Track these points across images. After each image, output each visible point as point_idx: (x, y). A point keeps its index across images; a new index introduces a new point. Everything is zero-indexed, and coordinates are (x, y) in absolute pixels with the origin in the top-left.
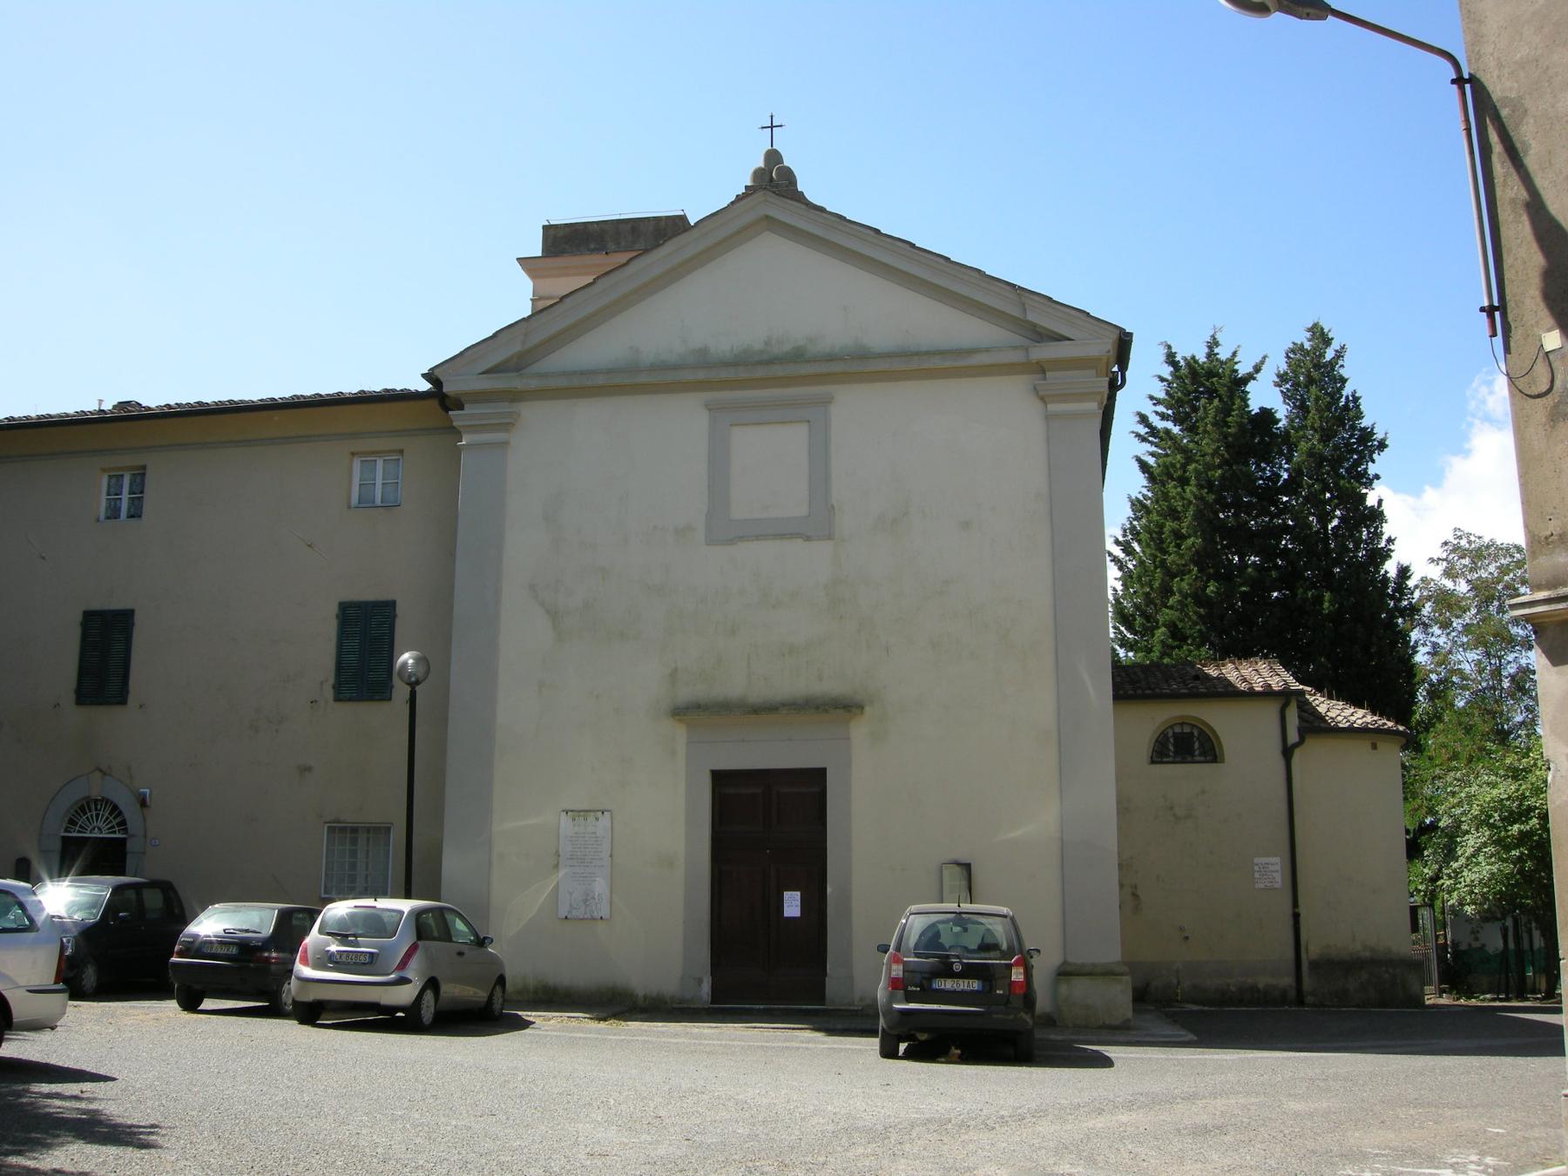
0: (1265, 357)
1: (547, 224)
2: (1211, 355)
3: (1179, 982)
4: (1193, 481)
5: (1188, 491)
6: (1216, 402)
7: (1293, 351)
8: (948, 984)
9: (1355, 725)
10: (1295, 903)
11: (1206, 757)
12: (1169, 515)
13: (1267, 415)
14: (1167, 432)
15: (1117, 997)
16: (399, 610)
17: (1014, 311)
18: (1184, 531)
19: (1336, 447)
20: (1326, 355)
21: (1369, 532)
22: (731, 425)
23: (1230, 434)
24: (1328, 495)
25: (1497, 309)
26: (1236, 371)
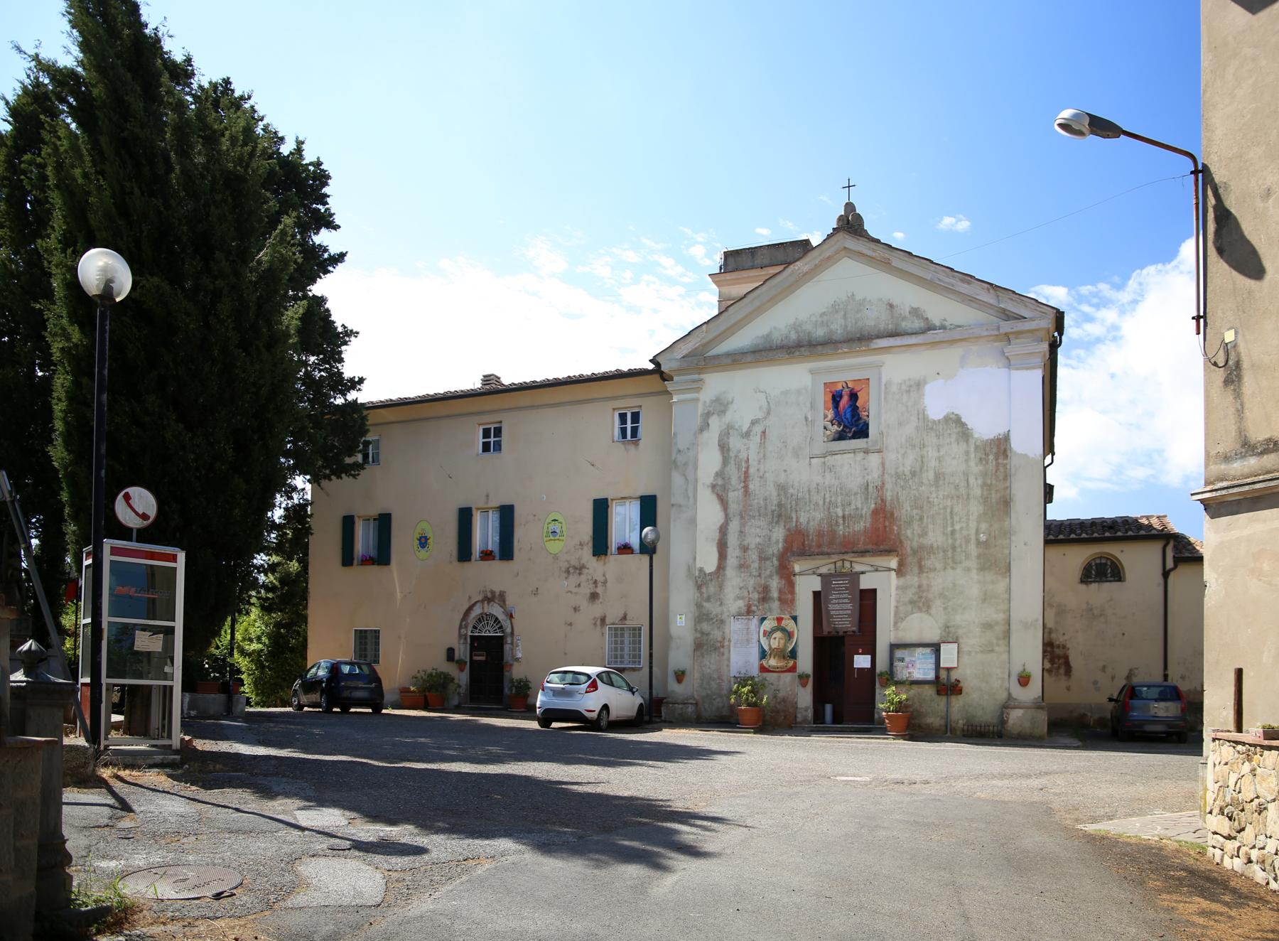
10: (1166, 667)
25: (1202, 317)
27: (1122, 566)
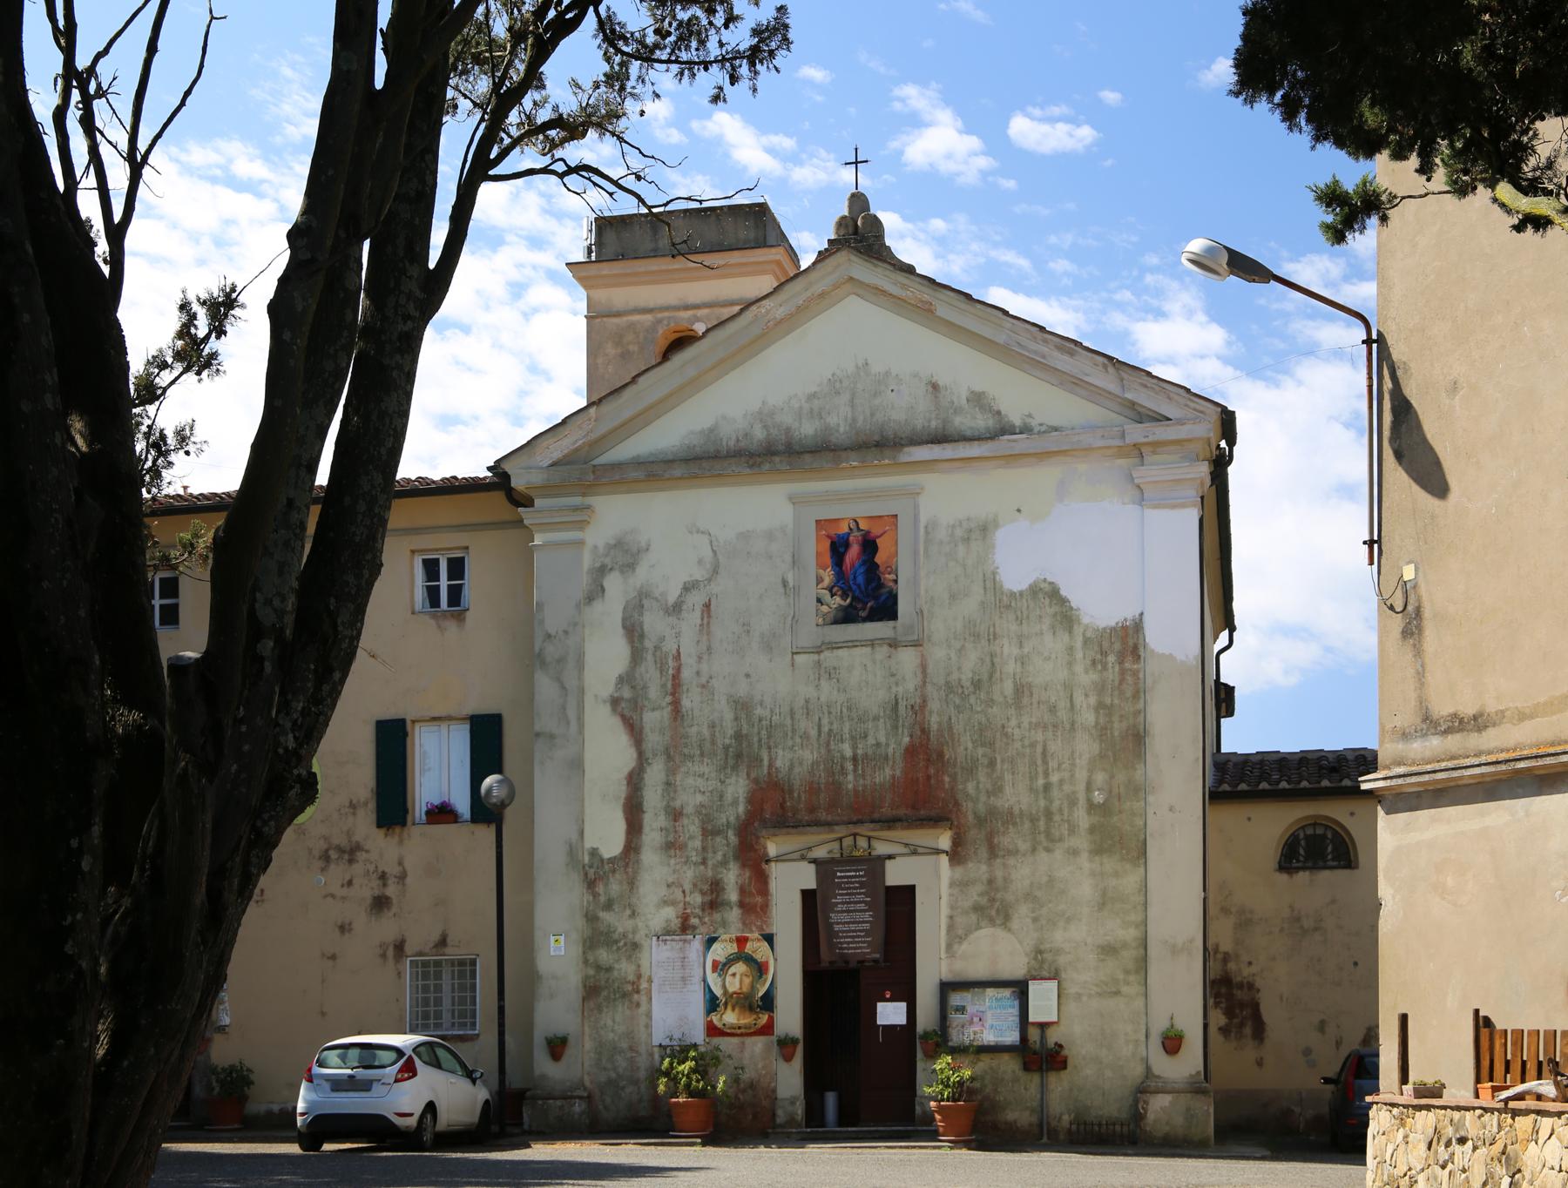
25: (1376, 542)
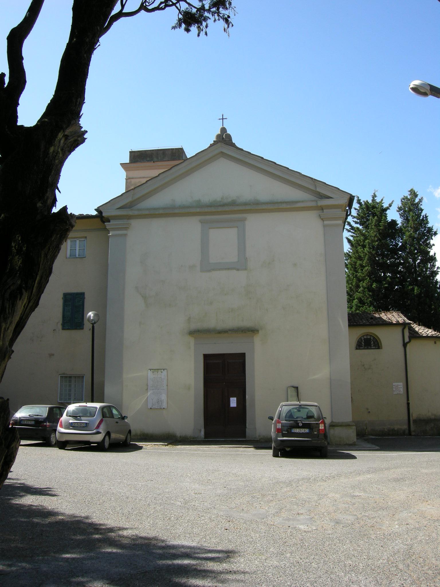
0: (393, 201)
1: (131, 151)
2: (373, 200)
3: (367, 428)
4: (367, 246)
5: (365, 250)
6: (376, 218)
7: (404, 199)
8: (297, 431)
9: (429, 335)
10: (408, 399)
11: (375, 346)
12: (358, 258)
13: (394, 222)
14: (358, 228)
15: (351, 434)
16: (86, 296)
17: (312, 188)
18: (364, 264)
19: (419, 234)
20: (416, 201)
21: (431, 265)
22: (209, 228)
23: (381, 229)
24: (416, 251)
26: (383, 206)
27: (381, 342)
